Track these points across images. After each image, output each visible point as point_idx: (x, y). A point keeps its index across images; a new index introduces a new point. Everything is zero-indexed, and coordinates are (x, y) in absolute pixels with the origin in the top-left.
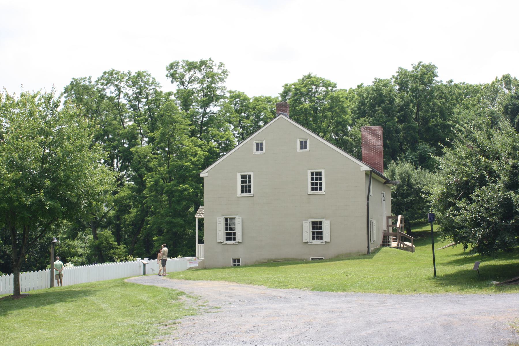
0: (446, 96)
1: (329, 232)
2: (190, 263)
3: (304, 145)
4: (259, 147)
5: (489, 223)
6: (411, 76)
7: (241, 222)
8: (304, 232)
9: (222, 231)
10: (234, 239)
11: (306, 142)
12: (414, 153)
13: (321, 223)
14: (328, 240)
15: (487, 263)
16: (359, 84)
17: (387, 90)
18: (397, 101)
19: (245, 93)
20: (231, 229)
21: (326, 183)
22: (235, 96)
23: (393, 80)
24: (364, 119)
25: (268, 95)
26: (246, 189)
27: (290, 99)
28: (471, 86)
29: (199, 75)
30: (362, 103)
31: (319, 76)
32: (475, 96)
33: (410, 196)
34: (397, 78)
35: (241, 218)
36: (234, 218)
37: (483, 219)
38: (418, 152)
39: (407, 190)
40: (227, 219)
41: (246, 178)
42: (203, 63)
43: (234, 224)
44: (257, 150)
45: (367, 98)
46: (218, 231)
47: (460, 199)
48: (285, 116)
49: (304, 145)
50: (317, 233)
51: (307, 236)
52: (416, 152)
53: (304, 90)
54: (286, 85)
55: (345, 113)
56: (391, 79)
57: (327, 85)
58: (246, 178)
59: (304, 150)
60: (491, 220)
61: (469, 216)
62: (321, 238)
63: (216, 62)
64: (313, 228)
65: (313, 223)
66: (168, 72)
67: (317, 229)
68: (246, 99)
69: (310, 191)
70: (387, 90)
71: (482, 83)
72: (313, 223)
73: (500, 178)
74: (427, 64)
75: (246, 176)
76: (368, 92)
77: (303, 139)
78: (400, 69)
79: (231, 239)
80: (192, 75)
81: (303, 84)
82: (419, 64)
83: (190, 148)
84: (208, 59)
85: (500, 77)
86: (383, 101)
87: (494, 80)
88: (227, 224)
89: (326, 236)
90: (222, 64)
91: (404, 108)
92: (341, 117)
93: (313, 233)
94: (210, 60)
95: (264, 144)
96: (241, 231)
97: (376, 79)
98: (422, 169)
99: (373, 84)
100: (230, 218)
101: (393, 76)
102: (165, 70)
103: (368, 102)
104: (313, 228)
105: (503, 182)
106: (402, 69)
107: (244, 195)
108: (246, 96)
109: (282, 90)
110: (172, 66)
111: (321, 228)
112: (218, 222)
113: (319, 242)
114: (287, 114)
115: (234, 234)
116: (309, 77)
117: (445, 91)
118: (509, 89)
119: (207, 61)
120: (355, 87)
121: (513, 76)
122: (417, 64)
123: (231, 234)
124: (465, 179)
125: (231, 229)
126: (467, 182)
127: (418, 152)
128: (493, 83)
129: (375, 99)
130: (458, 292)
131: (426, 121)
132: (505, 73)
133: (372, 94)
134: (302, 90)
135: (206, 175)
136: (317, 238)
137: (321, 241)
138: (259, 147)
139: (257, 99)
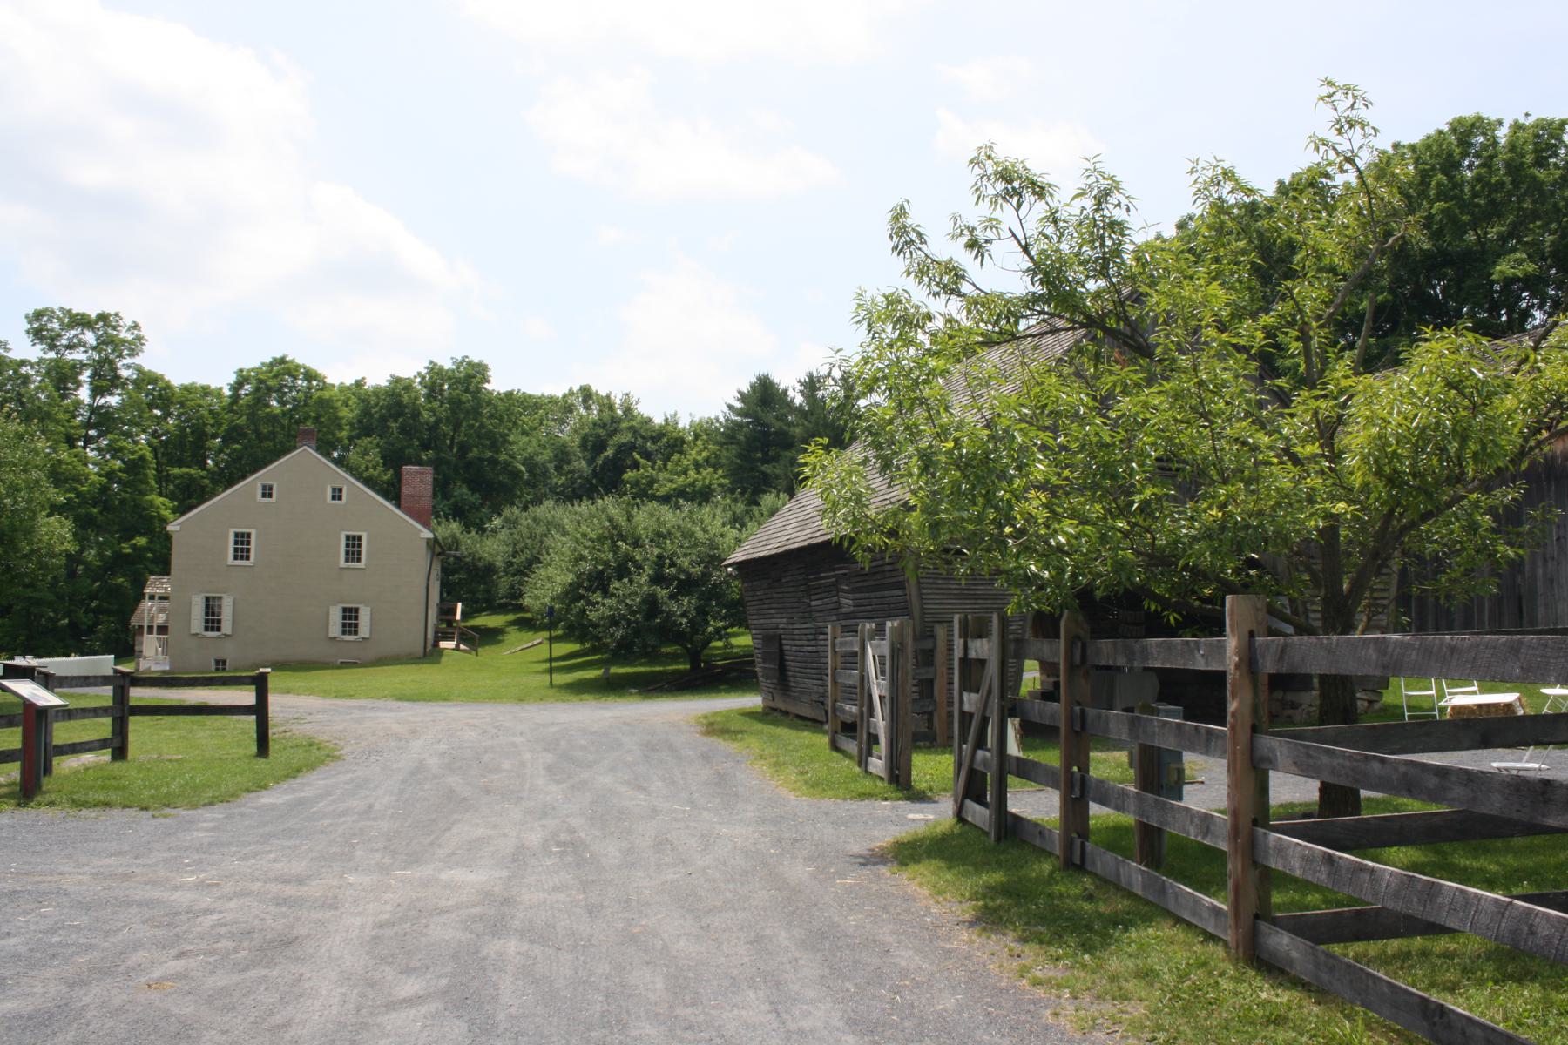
0: (501, 416)
1: (369, 624)
2: (157, 663)
3: (337, 494)
4: (267, 492)
5: (629, 622)
6: (450, 378)
7: (231, 604)
8: (331, 623)
9: (199, 617)
10: (219, 629)
11: (340, 490)
12: (446, 502)
13: (357, 610)
14: (367, 636)
15: (675, 667)
16: (359, 378)
17: (410, 397)
18: (425, 415)
19: (167, 378)
20: (213, 614)
21: (368, 551)
22: (145, 379)
23: (418, 380)
24: (369, 439)
25: (204, 383)
26: (242, 553)
27: (246, 395)
28: (530, 396)
29: (90, 337)
30: (366, 412)
31: (299, 361)
32: (536, 413)
33: (458, 573)
34: (424, 378)
35: (232, 598)
36: (220, 598)
37: (623, 617)
38: (453, 500)
39: (455, 563)
40: (207, 599)
41: (243, 537)
42: (103, 317)
43: (220, 607)
44: (264, 495)
45: (377, 405)
46: (193, 617)
47: (594, 592)
48: (311, 448)
49: (337, 494)
50: (350, 624)
51: (335, 629)
52: (448, 500)
53: (271, 383)
54: (241, 370)
55: (340, 428)
56: (415, 377)
57: (310, 376)
58: (243, 537)
59: (337, 502)
60: (632, 618)
61: (608, 613)
62: (356, 633)
63: (127, 321)
64: (344, 618)
65: (345, 610)
66: (29, 326)
67: (350, 618)
68: (168, 386)
69: (342, 563)
70: (410, 397)
71: (546, 395)
72: (345, 610)
73: (644, 571)
74: (476, 361)
75: (243, 534)
76: (378, 397)
77: (338, 485)
78: (431, 362)
79: (212, 630)
80: (76, 336)
81: (271, 372)
82: (463, 360)
83: (74, 468)
84: (112, 312)
85: (575, 389)
86: (402, 414)
87: (567, 392)
88: (207, 607)
89: (364, 629)
90: (136, 326)
91: (434, 428)
92: (334, 435)
93: (344, 625)
94: (117, 315)
95: (275, 488)
96: (230, 618)
97: (392, 376)
98: (477, 533)
99: (387, 384)
100: (214, 598)
101: (419, 374)
102: (25, 321)
103: (376, 412)
104: (344, 618)
105: (648, 575)
106: (436, 364)
107: (238, 562)
108: (169, 381)
109: (232, 378)
110: (38, 315)
111: (356, 618)
112: (193, 603)
113: (352, 638)
114: (314, 445)
115: (219, 622)
116: (282, 361)
117: (501, 407)
118: (587, 408)
119: (111, 315)
120: (349, 381)
121: (594, 389)
122: (460, 359)
123: (213, 621)
124: (600, 567)
125: (213, 614)
126: (602, 572)
127: (453, 500)
128: (565, 396)
129: (389, 408)
130: (594, 703)
131: (464, 448)
132: (584, 383)
133: (384, 400)
134: (268, 383)
135: (178, 528)
136: (350, 633)
137: (355, 637)
138: (267, 492)
139: (187, 389)
